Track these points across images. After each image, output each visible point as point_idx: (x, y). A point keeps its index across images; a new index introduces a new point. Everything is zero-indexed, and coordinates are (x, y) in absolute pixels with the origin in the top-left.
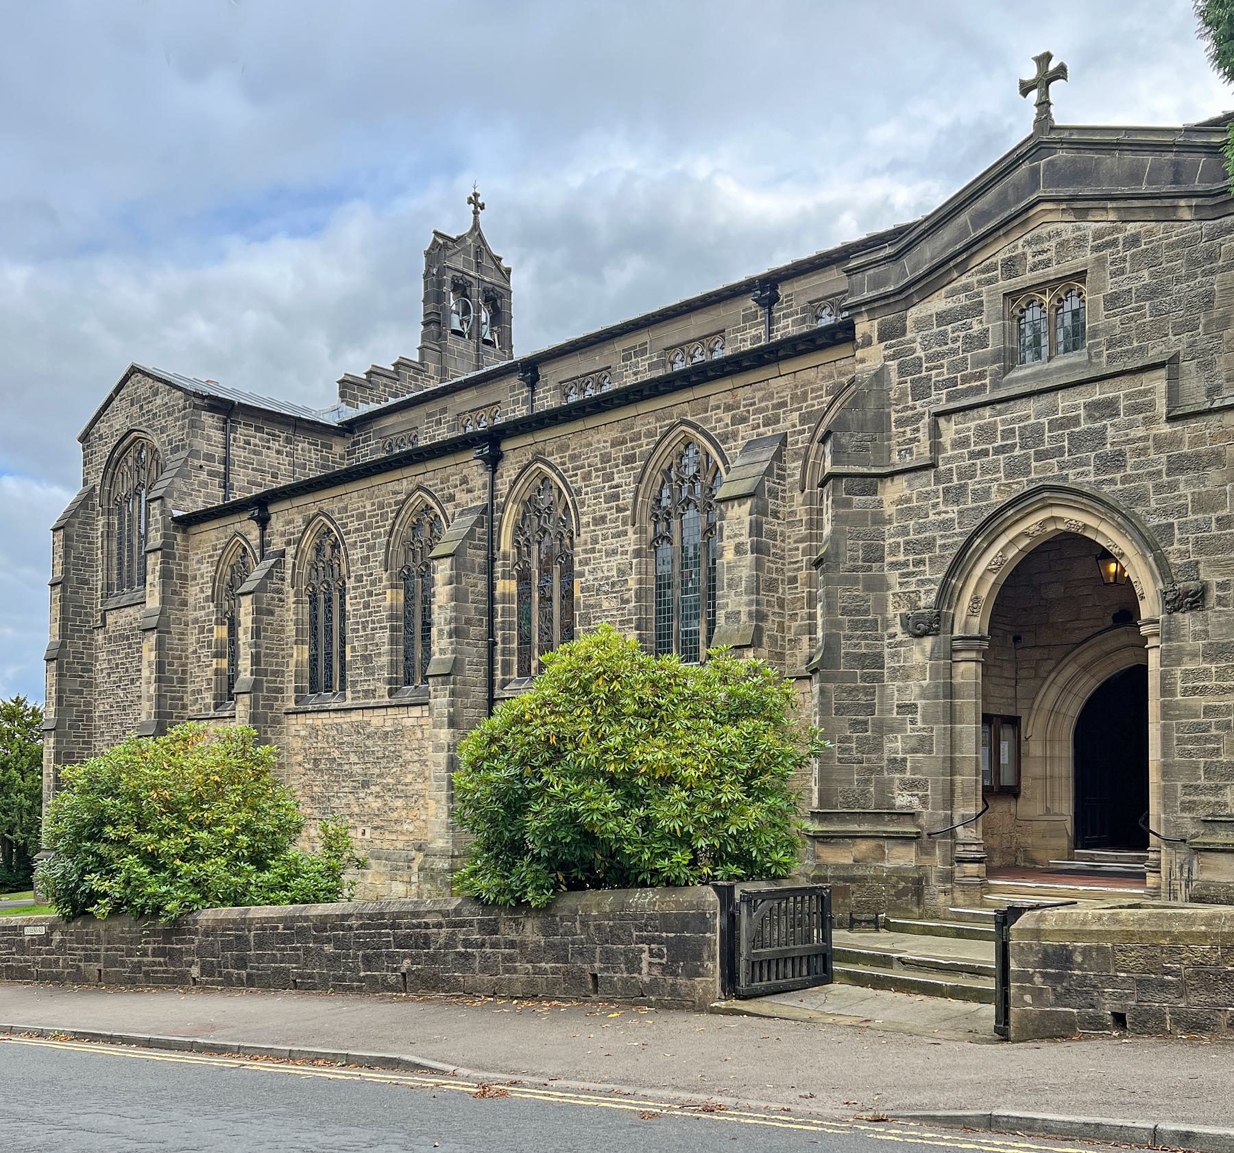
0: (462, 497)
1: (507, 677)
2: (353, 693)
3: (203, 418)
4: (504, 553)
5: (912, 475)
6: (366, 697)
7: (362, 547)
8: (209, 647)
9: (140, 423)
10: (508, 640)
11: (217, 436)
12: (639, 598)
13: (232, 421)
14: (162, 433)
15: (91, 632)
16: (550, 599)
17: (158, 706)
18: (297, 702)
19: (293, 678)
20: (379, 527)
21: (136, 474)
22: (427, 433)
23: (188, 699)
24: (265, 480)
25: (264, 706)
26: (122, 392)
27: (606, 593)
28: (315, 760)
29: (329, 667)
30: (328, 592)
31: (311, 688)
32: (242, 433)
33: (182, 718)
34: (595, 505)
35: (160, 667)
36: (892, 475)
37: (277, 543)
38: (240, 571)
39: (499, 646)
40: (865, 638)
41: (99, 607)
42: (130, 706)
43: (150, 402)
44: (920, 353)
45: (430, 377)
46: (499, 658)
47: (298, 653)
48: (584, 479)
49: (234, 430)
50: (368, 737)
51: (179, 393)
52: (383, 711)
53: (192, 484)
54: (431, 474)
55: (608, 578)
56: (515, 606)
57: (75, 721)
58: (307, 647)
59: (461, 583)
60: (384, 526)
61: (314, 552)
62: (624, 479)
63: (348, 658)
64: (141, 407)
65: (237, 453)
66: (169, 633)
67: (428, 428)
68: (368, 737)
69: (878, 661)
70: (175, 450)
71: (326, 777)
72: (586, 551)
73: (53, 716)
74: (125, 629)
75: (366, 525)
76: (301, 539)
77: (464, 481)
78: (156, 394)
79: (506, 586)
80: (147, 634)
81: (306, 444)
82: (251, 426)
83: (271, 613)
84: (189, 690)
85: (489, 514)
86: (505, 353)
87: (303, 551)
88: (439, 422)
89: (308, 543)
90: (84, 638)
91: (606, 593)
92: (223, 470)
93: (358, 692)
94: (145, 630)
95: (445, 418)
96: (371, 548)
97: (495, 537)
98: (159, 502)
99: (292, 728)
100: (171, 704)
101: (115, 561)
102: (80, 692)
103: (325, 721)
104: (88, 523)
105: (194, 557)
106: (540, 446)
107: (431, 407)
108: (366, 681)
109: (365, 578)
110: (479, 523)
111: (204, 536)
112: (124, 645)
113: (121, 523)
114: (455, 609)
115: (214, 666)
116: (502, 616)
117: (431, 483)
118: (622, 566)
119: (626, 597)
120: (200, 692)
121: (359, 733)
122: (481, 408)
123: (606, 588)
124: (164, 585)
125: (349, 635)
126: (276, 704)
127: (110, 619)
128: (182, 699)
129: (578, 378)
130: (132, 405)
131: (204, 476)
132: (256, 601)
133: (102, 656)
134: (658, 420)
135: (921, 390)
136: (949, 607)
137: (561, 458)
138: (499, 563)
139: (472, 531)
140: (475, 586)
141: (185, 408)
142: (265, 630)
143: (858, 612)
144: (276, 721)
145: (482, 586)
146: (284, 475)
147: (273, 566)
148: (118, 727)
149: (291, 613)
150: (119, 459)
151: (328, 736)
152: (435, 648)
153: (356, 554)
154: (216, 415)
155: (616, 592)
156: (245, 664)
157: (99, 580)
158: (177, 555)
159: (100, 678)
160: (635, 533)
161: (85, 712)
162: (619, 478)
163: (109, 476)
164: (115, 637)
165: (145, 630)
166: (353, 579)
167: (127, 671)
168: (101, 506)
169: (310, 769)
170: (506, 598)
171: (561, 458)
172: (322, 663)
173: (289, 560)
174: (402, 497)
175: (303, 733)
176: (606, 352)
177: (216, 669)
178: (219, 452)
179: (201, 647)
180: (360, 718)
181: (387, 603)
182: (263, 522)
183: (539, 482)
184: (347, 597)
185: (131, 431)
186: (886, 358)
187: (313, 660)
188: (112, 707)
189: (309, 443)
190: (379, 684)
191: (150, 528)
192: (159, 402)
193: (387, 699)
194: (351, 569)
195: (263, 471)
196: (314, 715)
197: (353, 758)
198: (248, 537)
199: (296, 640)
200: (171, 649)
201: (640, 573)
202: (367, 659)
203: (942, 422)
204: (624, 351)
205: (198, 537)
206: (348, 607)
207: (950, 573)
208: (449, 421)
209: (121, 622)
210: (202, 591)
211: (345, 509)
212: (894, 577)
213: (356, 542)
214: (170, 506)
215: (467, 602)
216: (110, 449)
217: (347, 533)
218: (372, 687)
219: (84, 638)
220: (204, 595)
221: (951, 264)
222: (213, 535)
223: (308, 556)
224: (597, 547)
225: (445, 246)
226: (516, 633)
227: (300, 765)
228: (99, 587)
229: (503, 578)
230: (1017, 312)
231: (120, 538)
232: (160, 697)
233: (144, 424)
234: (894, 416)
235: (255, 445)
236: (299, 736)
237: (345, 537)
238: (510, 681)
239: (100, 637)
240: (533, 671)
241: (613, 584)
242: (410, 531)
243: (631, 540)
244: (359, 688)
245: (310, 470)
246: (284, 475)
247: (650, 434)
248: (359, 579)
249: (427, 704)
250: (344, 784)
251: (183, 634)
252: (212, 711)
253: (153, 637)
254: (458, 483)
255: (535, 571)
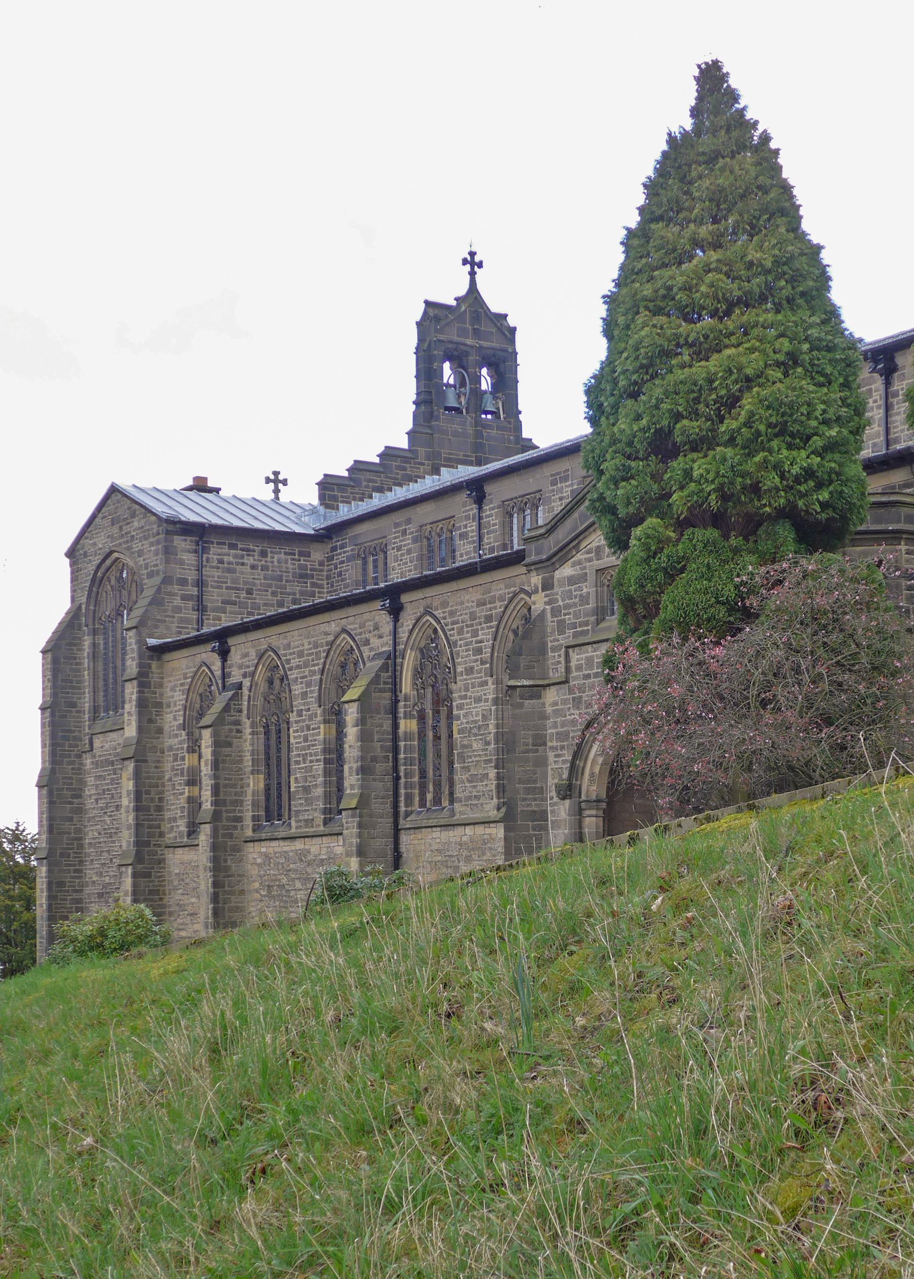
0: (375, 642)
1: (409, 809)
2: (297, 822)
3: (175, 543)
4: (406, 695)
5: (558, 686)
6: (306, 826)
7: (301, 683)
8: (182, 774)
9: (120, 544)
10: (409, 772)
11: (189, 558)
12: (497, 742)
13: (206, 542)
14: (139, 556)
15: (79, 756)
16: (439, 738)
17: (137, 835)
18: (254, 831)
19: (250, 808)
20: (314, 665)
21: (118, 595)
22: (394, 543)
23: (165, 827)
24: (238, 597)
25: (224, 835)
26: (104, 509)
27: (475, 735)
28: (269, 886)
29: (280, 796)
30: (278, 725)
31: (266, 816)
32: (215, 552)
33: (160, 846)
34: (466, 657)
35: (138, 795)
36: (549, 685)
37: (236, 676)
38: (206, 699)
39: (403, 780)
40: (535, 799)
41: (87, 730)
42: (116, 833)
43: (128, 524)
44: (561, 603)
45: (420, 464)
46: (402, 791)
47: (254, 783)
48: (459, 634)
49: (205, 550)
50: (309, 864)
51: (153, 518)
52: (319, 839)
53: (165, 611)
54: (352, 618)
55: (476, 722)
56: (416, 743)
57: (66, 849)
58: (262, 776)
59: (366, 725)
60: (318, 664)
61: (267, 685)
62: (485, 635)
63: (292, 789)
64: (121, 528)
65: (212, 574)
66: (146, 761)
67: (395, 538)
68: (309, 864)
69: (543, 816)
70: (151, 575)
71: (277, 903)
72: (461, 698)
73: (44, 845)
74: (110, 754)
75: (304, 662)
76: (254, 673)
77: (376, 628)
78: (133, 515)
79: (408, 725)
80: (127, 763)
81: (282, 556)
82: (224, 544)
83: (230, 745)
84: (166, 817)
85: (392, 661)
86: (510, 423)
87: (256, 685)
88: (404, 533)
89: (261, 674)
90: (72, 763)
91: (475, 735)
92: (196, 593)
93: (300, 821)
94: (123, 759)
95: (409, 529)
96: (309, 685)
97: (398, 680)
98: (134, 631)
99: (251, 856)
100: (149, 833)
101: (101, 683)
102: (71, 819)
103: (276, 850)
104: (75, 643)
105: (168, 685)
106: (429, 601)
107: (397, 517)
108: (306, 810)
109: (304, 713)
110: (384, 668)
111: (175, 664)
112: (110, 770)
113: (106, 644)
114: (362, 748)
115: (187, 794)
116: (405, 753)
117: (352, 627)
118: (485, 712)
119: (488, 739)
120: (175, 819)
121: (302, 860)
122: (439, 521)
123: (475, 731)
124: (140, 714)
125: (293, 767)
126: (236, 833)
127: (97, 743)
128: (159, 827)
129: (516, 498)
130: (113, 525)
131: (178, 601)
132: (215, 735)
133: (90, 780)
134: (506, 587)
135: (561, 627)
136: (577, 780)
137: (444, 613)
138: (402, 704)
139: (377, 676)
140: (381, 726)
141: (158, 534)
142: (224, 762)
143: (529, 782)
144: (237, 849)
145: (387, 725)
146: (259, 590)
147: (230, 699)
148: (105, 855)
149: (248, 743)
150: (102, 578)
151: (278, 863)
152: (346, 784)
153: (297, 689)
154: (189, 538)
155: (482, 735)
156: (207, 795)
157: (86, 703)
158: (153, 684)
159: (89, 803)
160: (493, 684)
161: (76, 839)
162: (483, 634)
163: (93, 595)
164: (102, 761)
165: (123, 759)
166: (295, 713)
167: (113, 797)
168: (87, 626)
169: (264, 896)
170: (408, 736)
171: (444, 613)
172: (274, 793)
173: (245, 691)
174: (331, 638)
175: (259, 861)
176: (538, 476)
177: (189, 797)
178: (192, 576)
179: (176, 775)
180: (302, 846)
181: (321, 737)
182: (224, 653)
183: (431, 631)
184: (291, 730)
185: (111, 552)
186: (546, 603)
187: (268, 789)
188: (100, 834)
189: (286, 553)
190: (316, 814)
191: (128, 657)
192: (136, 524)
193: (322, 828)
194: (294, 703)
195: (238, 589)
196: (267, 843)
197: (298, 885)
198: (213, 668)
199: (253, 770)
200: (149, 778)
201: (497, 719)
202: (306, 789)
203: (570, 651)
204: (552, 475)
205: (171, 664)
206: (292, 741)
207: (575, 756)
208: (412, 533)
209: (107, 746)
210: (175, 719)
211: (288, 646)
212: (551, 755)
213: (297, 678)
214: (144, 635)
215: (372, 741)
216: (94, 568)
217: (290, 669)
218: (311, 817)
219: (72, 763)
220: (176, 723)
221: (571, 545)
222: (184, 663)
223: (262, 688)
224: (469, 694)
225: (437, 319)
226: (416, 767)
227: (257, 892)
228: (87, 709)
229: (405, 718)
230: (606, 581)
231: (105, 659)
232: (138, 826)
233: (124, 546)
234: (550, 645)
235: (229, 563)
236: (256, 863)
237: (289, 673)
238: (412, 812)
239: (88, 761)
240: (428, 804)
241: (479, 728)
242: (339, 669)
243: (490, 691)
244: (301, 818)
245: (287, 581)
246: (259, 590)
247: (501, 599)
248: (300, 713)
249: (341, 834)
250: (291, 909)
251: (158, 762)
252: (185, 839)
253: (131, 766)
254: (372, 628)
255: (429, 712)
